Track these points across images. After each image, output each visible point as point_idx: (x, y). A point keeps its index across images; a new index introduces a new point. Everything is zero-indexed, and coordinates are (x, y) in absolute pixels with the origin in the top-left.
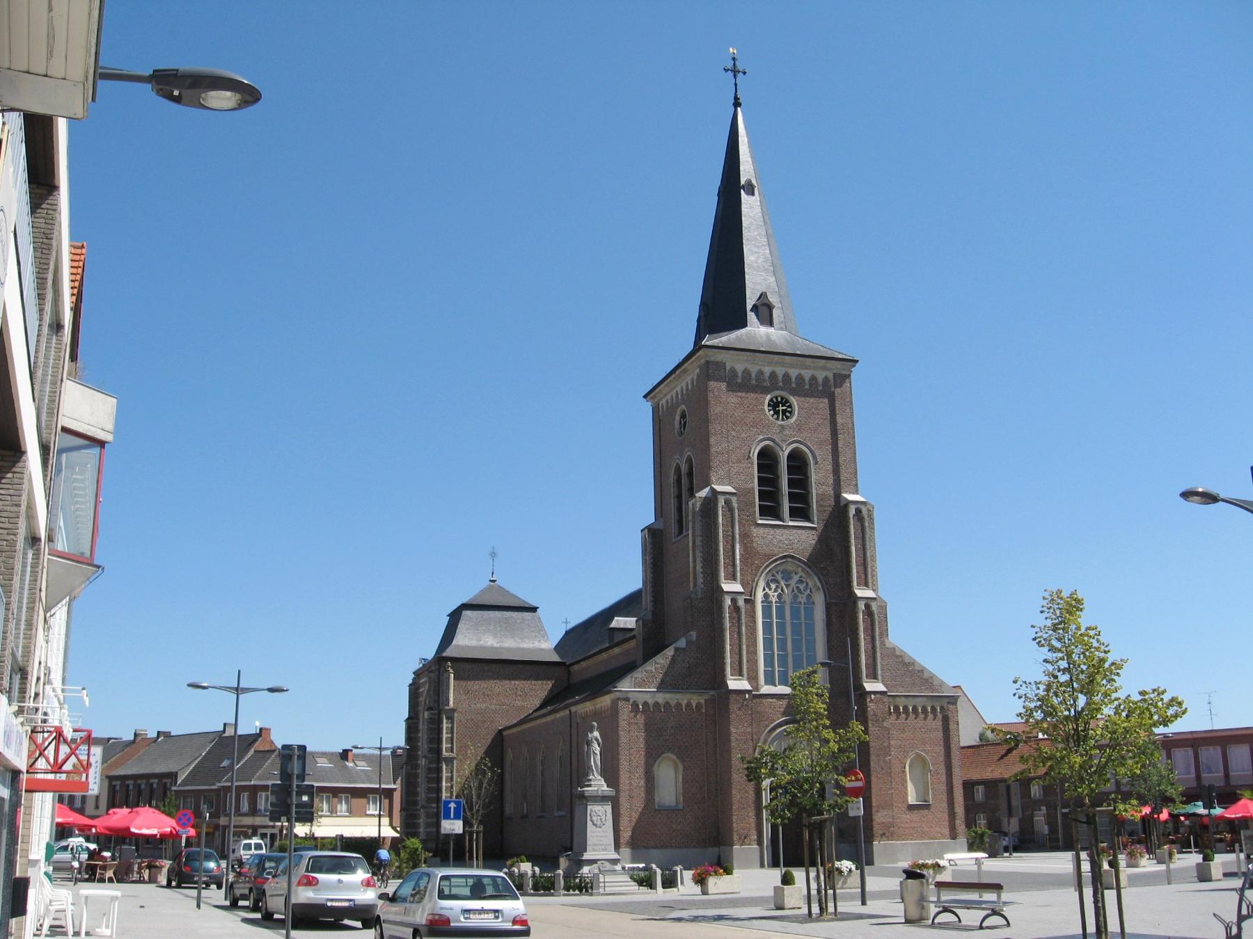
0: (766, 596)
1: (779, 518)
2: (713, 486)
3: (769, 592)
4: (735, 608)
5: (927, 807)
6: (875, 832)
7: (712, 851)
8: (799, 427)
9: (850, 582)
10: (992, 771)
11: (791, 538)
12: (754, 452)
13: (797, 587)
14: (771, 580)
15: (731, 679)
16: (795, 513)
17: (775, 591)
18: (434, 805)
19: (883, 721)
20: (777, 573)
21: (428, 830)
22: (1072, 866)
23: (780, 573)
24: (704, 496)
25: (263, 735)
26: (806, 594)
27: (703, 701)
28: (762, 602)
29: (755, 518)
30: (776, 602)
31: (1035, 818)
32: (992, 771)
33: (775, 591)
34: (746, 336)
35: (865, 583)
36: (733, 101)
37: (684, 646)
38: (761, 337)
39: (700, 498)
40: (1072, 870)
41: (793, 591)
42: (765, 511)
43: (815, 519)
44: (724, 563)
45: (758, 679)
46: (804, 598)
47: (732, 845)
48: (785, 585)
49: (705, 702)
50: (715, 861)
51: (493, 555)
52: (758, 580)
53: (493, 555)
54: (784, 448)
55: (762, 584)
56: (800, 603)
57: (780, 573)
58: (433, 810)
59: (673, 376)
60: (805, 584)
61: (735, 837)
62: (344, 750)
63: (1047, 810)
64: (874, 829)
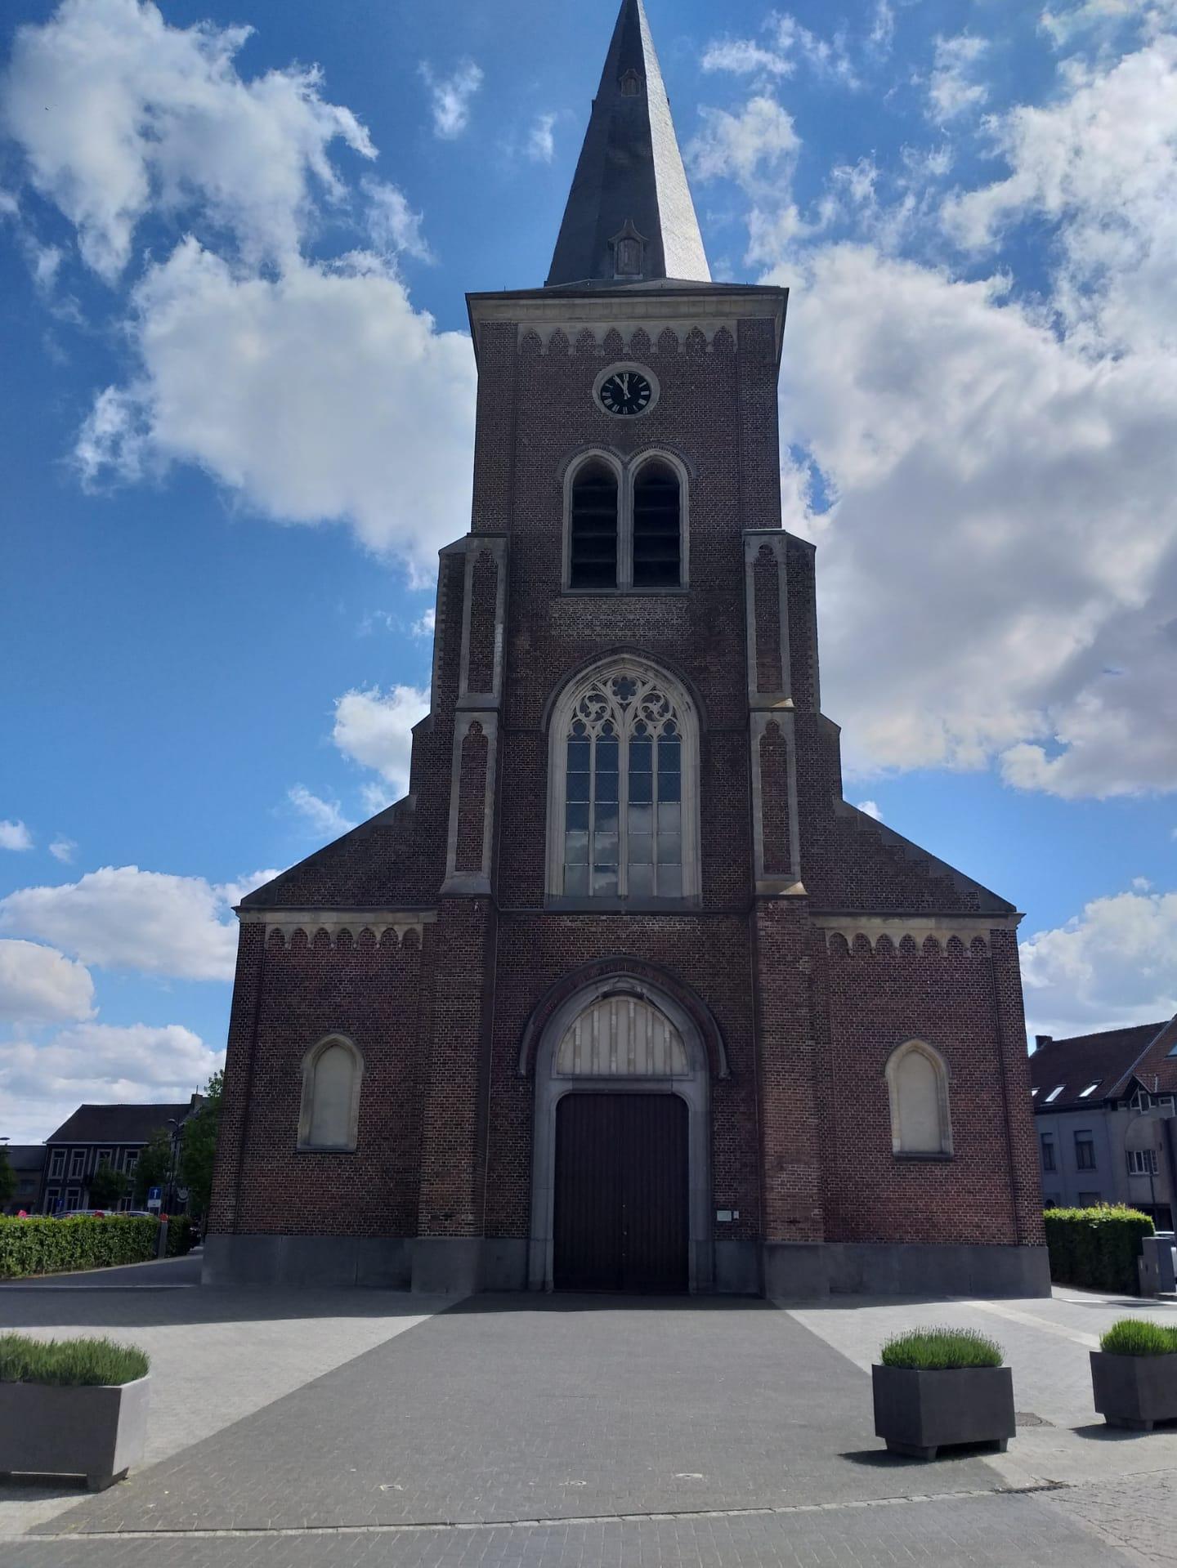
0: (579, 726)
3: (584, 720)
11: (632, 617)
14: (591, 698)
23: (610, 683)
28: (570, 738)
52: (557, 696)
57: (610, 683)
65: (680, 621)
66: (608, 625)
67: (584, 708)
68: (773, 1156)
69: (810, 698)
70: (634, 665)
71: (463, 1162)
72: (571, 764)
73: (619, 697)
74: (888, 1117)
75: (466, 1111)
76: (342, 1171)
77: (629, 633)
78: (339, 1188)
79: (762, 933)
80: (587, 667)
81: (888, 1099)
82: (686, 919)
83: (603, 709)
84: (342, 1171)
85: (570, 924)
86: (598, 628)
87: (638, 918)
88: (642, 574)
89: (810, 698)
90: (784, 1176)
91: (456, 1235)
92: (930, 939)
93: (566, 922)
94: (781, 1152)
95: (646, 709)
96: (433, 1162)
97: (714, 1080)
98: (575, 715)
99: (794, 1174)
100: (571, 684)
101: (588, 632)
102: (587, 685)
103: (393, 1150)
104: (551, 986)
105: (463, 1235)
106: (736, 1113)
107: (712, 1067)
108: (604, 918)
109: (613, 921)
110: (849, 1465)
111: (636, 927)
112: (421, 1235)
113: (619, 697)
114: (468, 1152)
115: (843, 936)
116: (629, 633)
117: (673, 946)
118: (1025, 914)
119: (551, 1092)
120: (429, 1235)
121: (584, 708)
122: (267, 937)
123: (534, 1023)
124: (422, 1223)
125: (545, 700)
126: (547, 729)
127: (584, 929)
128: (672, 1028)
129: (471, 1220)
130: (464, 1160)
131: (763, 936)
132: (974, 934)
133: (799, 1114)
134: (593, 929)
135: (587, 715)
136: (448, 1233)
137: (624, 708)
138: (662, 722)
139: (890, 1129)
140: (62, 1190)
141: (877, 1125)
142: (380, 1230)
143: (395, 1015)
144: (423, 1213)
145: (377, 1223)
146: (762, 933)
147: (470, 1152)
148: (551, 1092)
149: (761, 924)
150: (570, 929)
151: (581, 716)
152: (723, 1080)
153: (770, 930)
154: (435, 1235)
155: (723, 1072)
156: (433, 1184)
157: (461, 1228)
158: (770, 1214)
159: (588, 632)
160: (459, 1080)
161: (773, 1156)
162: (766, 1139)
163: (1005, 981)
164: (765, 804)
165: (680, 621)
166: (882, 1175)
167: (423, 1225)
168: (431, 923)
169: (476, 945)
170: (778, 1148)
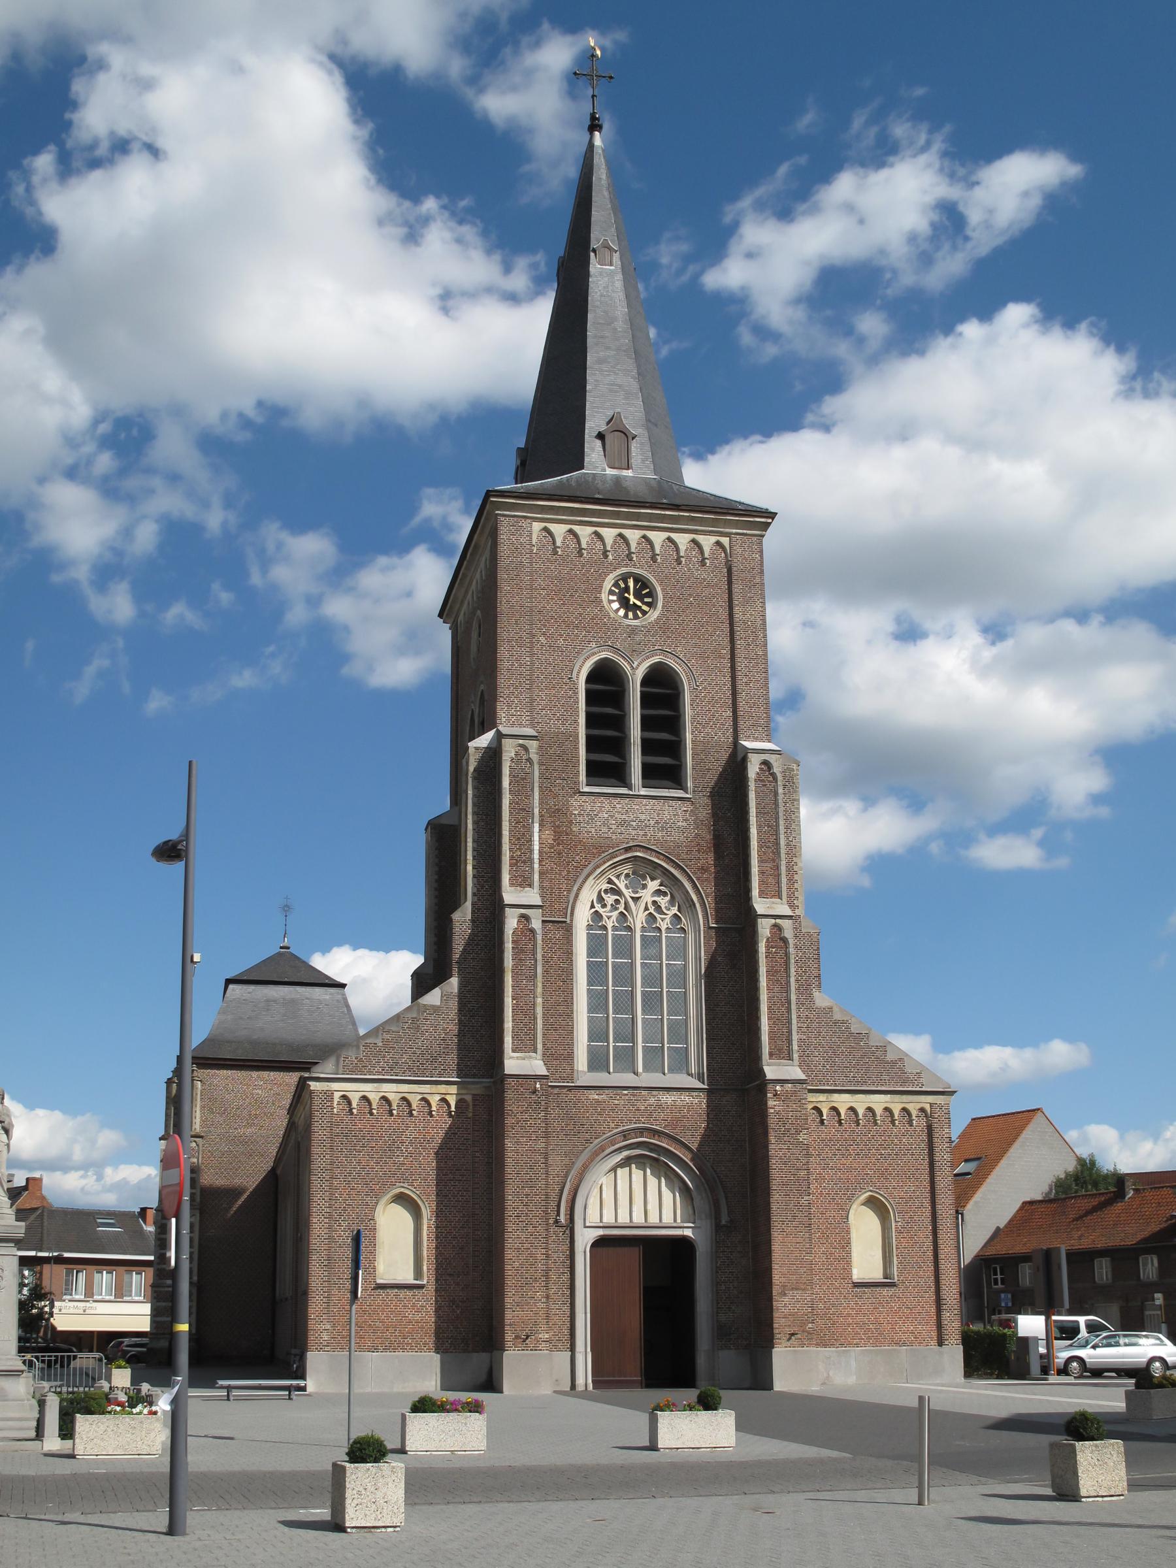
0: (597, 916)
1: (630, 787)
2: (500, 728)
3: (601, 911)
4: (526, 932)
5: (893, 1285)
6: (776, 1331)
7: (479, 1360)
8: (662, 626)
9: (748, 890)
10: (1080, 1238)
11: (643, 817)
12: (579, 672)
13: (654, 903)
14: (606, 891)
15: (511, 1058)
16: (652, 774)
17: (614, 908)
18: (169, 1282)
19: (798, 1132)
20: (618, 877)
21: (159, 1319)
22: (190, 1458)
23: (623, 877)
24: (486, 746)
25: (30, 1187)
26: (671, 913)
27: (469, 1098)
28: (589, 927)
29: (577, 783)
30: (614, 928)
31: (1147, 1313)
32: (1080, 1238)
33: (614, 908)
34: (577, 481)
35: (772, 891)
36: (588, 123)
37: (438, 1003)
38: (604, 482)
39: (477, 748)
40: (1125, 1408)
41: (646, 909)
42: (597, 771)
43: (690, 784)
44: (512, 858)
45: (573, 1060)
46: (668, 920)
47: (502, 1349)
48: (632, 898)
49: (474, 1100)
50: (483, 1377)
51: (286, 909)
52: (579, 889)
53: (286, 909)
54: (636, 663)
55: (588, 894)
56: (659, 930)
57: (623, 877)
58: (166, 1289)
59: (465, 563)
60: (668, 898)
61: (509, 1336)
62: (142, 1209)
63: (1165, 1299)
64: (775, 1325)
65: (684, 824)
66: (623, 823)
67: (600, 899)
68: (778, 1285)
69: (795, 902)
70: (644, 863)
71: (538, 1294)
72: (591, 952)
73: (630, 890)
74: (849, 1253)
75: (538, 1254)
76: (416, 1301)
77: (641, 833)
78: (414, 1315)
79: (772, 1111)
80: (605, 863)
81: (850, 1238)
82: (695, 1094)
83: (617, 901)
84: (416, 1301)
85: (596, 1097)
86: (614, 827)
87: (654, 1093)
88: (652, 774)
89: (795, 902)
90: (786, 1299)
91: (536, 1350)
92: (887, 1109)
93: (594, 1095)
94: (784, 1283)
95: (654, 903)
96: (514, 1295)
97: (718, 1228)
98: (592, 906)
99: (794, 1299)
100: (591, 878)
101: (605, 829)
102: (604, 879)
103: (458, 1284)
104: (584, 1150)
105: (541, 1350)
106: (734, 1252)
107: (717, 1215)
108: (625, 1092)
109: (634, 1095)
110: (986, 1430)
111: (652, 1100)
112: (508, 1350)
113: (630, 890)
114: (542, 1287)
115: (820, 1109)
116: (641, 833)
117: (684, 1117)
118: (956, 1092)
119: (585, 1238)
120: (514, 1350)
121: (600, 899)
122: (335, 1103)
123: (570, 1182)
124: (508, 1341)
125: (569, 891)
126: (572, 920)
127: (609, 1102)
128: (681, 1185)
129: (547, 1338)
130: (538, 1292)
131: (772, 1113)
132: (919, 1106)
133: (798, 1253)
134: (616, 1102)
135: (604, 906)
136: (529, 1349)
137: (636, 900)
138: (669, 916)
139: (851, 1261)
140: (991, 1288)
141: (841, 1259)
142: (451, 1347)
143: (451, 1173)
144: (508, 1333)
145: (447, 1341)
146: (772, 1111)
147: (542, 1287)
148: (585, 1238)
149: (771, 1103)
150: (597, 1101)
151: (598, 907)
152: (724, 1226)
153: (777, 1108)
154: (519, 1350)
155: (724, 1221)
156: (514, 1311)
157: (539, 1344)
158: (777, 1328)
159: (605, 829)
160: (530, 1229)
161: (778, 1285)
162: (773, 1273)
163: (940, 1145)
164: (769, 998)
165: (684, 824)
166: (845, 1296)
167: (509, 1343)
168: (479, 1095)
169: (539, 1119)
170: (783, 1280)
